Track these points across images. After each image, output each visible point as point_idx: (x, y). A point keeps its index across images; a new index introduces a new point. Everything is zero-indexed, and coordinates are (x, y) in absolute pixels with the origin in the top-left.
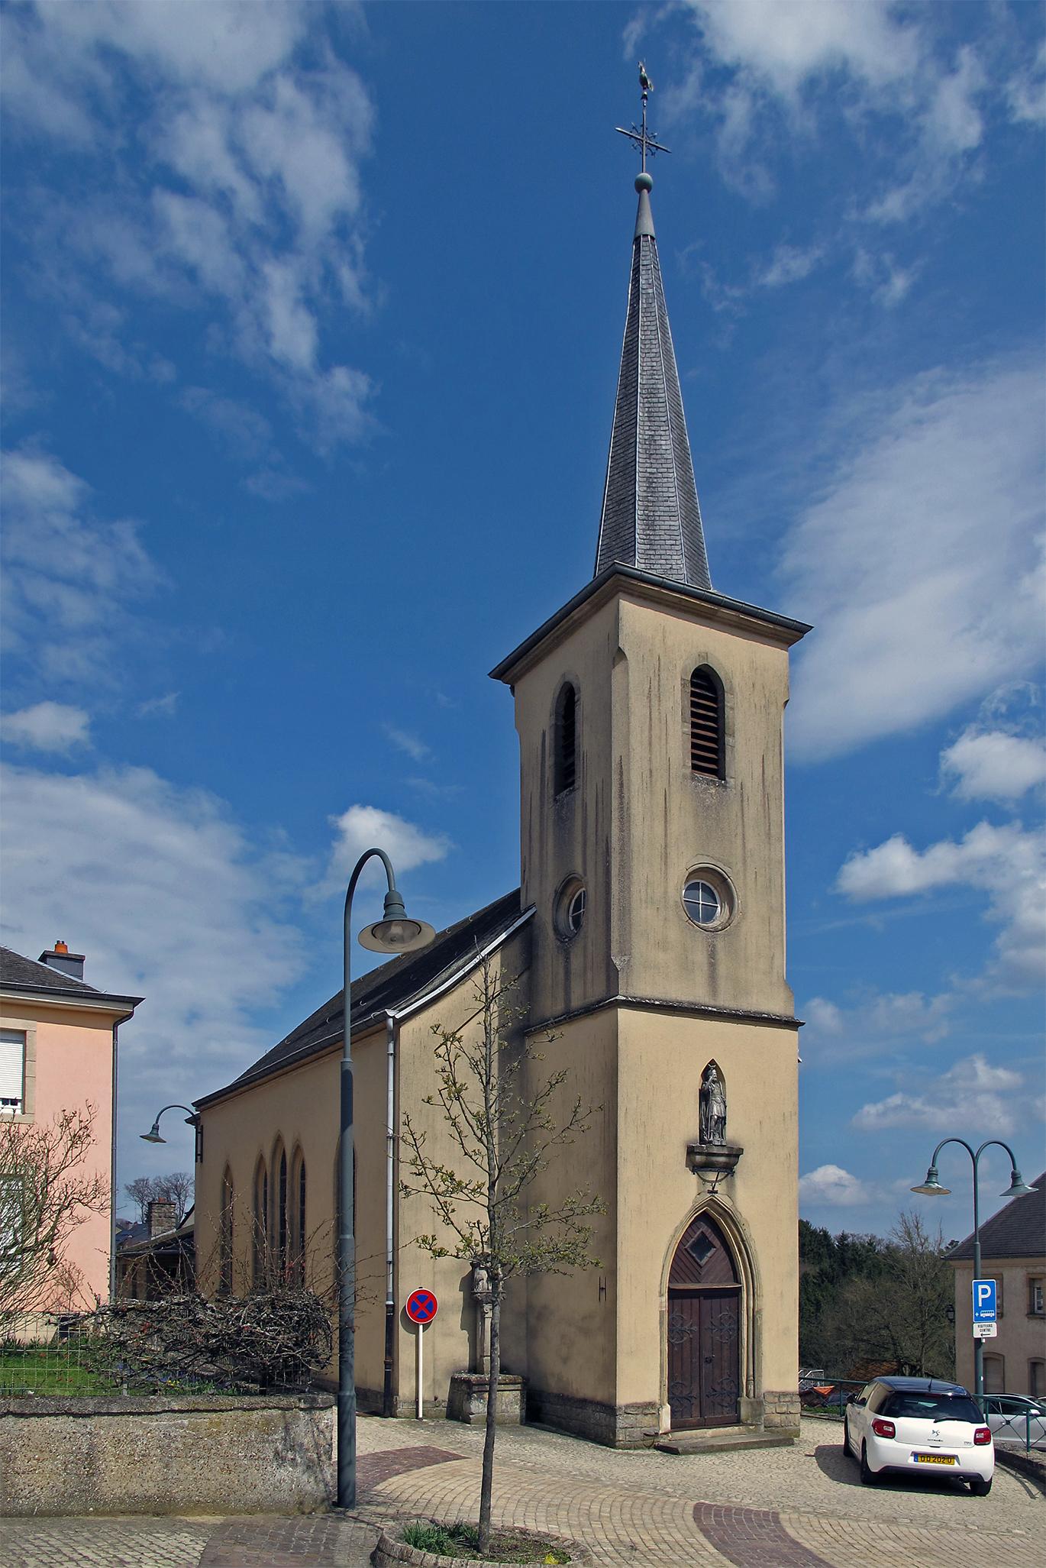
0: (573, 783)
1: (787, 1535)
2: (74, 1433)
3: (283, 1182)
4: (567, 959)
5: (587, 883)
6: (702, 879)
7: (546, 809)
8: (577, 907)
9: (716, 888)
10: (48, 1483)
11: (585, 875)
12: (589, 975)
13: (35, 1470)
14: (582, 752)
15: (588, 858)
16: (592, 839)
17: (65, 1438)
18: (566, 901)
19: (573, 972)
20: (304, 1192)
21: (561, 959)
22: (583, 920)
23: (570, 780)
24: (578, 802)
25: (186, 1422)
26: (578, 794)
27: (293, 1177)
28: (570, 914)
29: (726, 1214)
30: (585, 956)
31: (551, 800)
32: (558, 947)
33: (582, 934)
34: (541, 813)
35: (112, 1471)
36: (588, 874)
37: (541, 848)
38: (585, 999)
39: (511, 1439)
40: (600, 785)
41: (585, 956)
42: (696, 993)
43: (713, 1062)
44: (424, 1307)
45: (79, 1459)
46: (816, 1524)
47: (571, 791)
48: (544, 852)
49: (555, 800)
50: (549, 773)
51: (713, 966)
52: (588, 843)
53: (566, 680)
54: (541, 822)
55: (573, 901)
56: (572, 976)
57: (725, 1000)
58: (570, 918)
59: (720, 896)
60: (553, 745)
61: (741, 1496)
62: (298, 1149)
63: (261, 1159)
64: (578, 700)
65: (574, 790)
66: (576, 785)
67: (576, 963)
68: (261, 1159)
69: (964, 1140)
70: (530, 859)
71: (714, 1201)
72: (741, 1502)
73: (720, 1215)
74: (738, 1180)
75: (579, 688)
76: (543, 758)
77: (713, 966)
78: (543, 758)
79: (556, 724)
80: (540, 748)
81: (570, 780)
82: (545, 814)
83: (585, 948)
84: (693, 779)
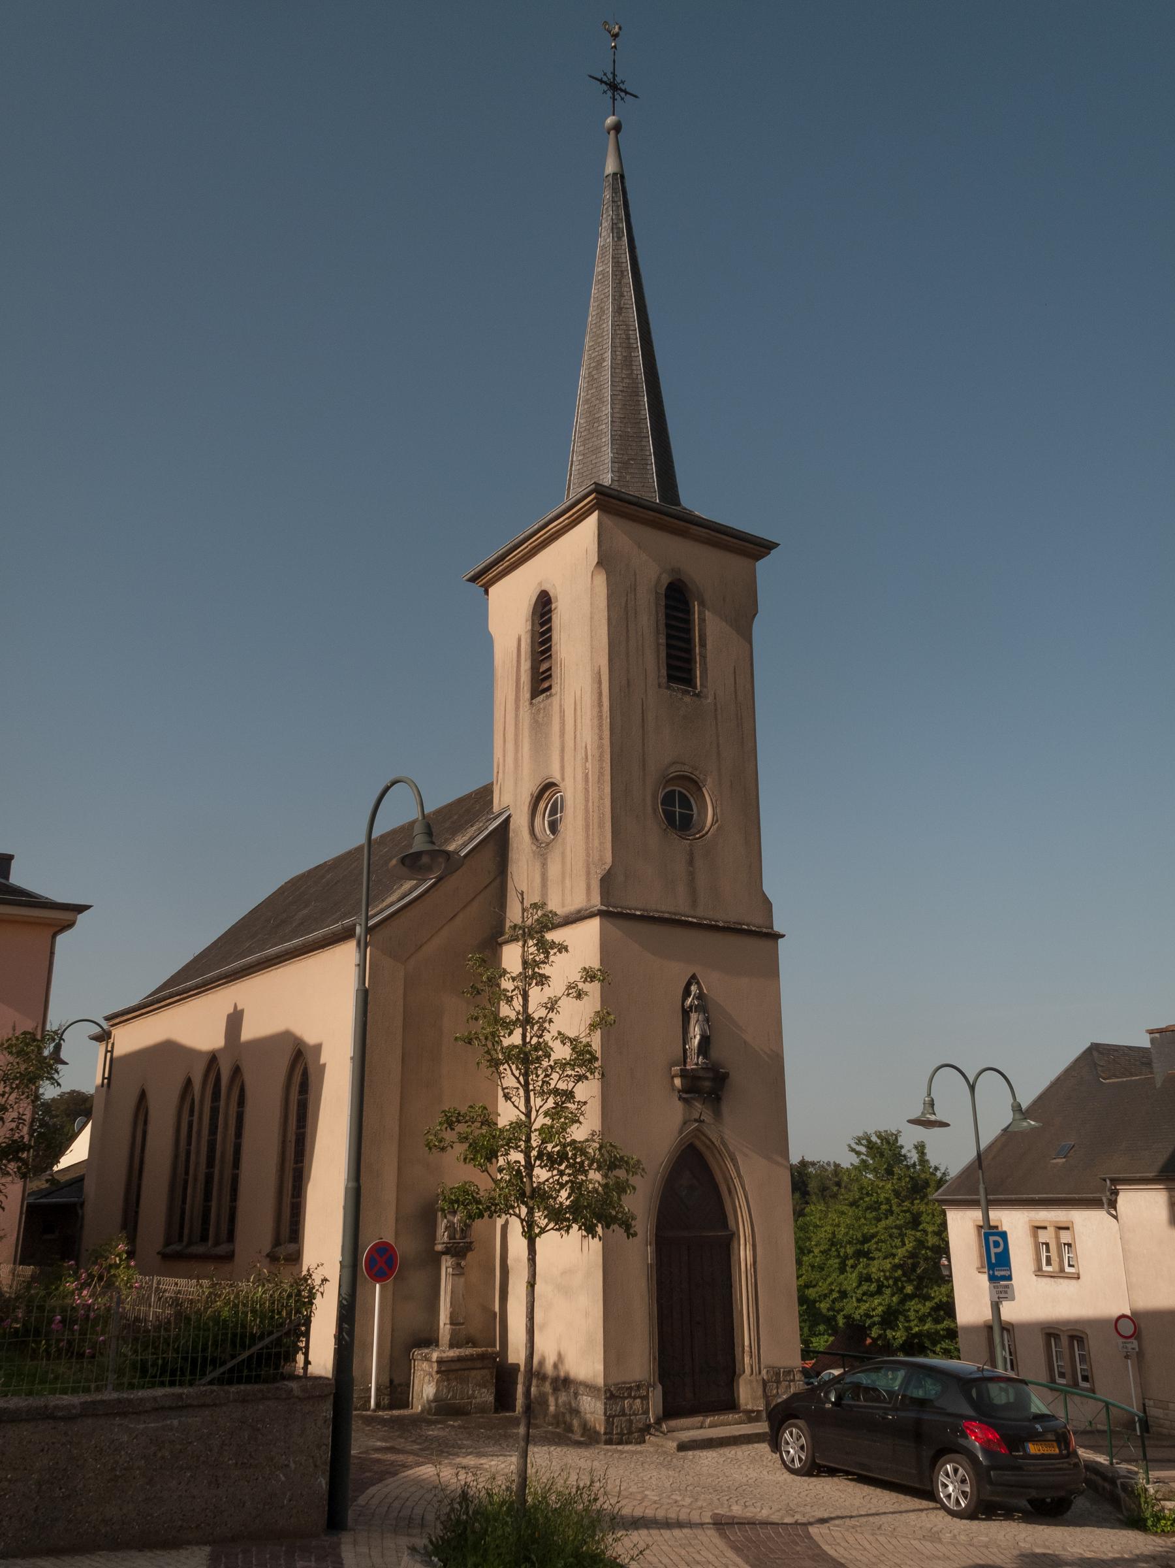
0: (549, 688)
1: (826, 1554)
2: (53, 1443)
3: (215, 1111)
4: (544, 865)
5: (566, 788)
6: (678, 786)
7: (521, 712)
8: (554, 811)
9: (692, 796)
10: (19, 1511)
11: (563, 779)
12: (568, 882)
13: (5, 1494)
14: (559, 659)
15: (566, 764)
16: (569, 744)
17: (42, 1450)
18: (542, 805)
19: (550, 878)
20: (304, 1127)
21: (538, 865)
22: (561, 827)
23: (546, 685)
24: (556, 708)
25: (176, 1422)
26: (555, 701)
27: (227, 1105)
28: (546, 818)
29: (711, 1146)
30: (563, 863)
31: (527, 703)
32: (534, 852)
33: (560, 840)
34: (517, 716)
35: (90, 1491)
36: (567, 779)
37: (516, 751)
38: (563, 907)
39: (482, 1433)
40: (578, 693)
41: (563, 863)
42: (676, 904)
43: (694, 977)
44: (928, 1298)
45: (55, 1478)
46: (851, 1540)
47: (548, 697)
48: (520, 755)
49: (531, 703)
50: (525, 678)
51: (692, 877)
52: (566, 749)
53: (543, 588)
54: (516, 725)
55: (549, 805)
56: (549, 883)
57: (705, 911)
58: (546, 823)
59: (696, 803)
60: (530, 650)
61: (759, 1504)
62: (237, 1071)
63: (189, 1083)
64: (555, 609)
65: (551, 695)
66: (553, 691)
67: (554, 869)
68: (189, 1083)
69: (937, 1066)
70: (504, 761)
71: (700, 1131)
72: (760, 1512)
73: (708, 1147)
74: (725, 1109)
75: (556, 597)
76: (519, 662)
77: (692, 877)
78: (519, 662)
79: (532, 630)
80: (515, 651)
81: (546, 685)
82: (521, 717)
83: (563, 854)
84: (668, 688)
